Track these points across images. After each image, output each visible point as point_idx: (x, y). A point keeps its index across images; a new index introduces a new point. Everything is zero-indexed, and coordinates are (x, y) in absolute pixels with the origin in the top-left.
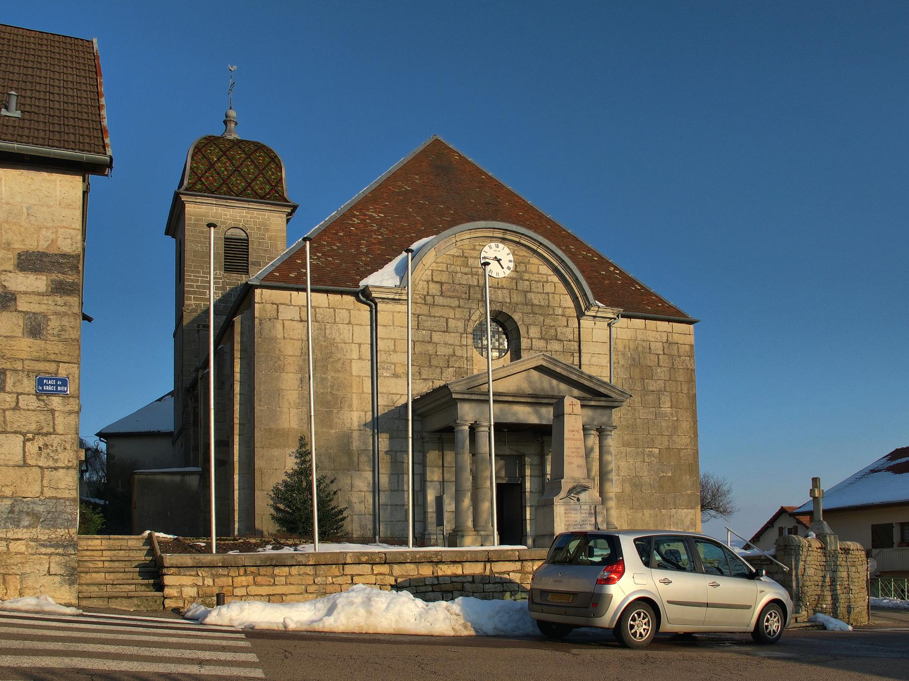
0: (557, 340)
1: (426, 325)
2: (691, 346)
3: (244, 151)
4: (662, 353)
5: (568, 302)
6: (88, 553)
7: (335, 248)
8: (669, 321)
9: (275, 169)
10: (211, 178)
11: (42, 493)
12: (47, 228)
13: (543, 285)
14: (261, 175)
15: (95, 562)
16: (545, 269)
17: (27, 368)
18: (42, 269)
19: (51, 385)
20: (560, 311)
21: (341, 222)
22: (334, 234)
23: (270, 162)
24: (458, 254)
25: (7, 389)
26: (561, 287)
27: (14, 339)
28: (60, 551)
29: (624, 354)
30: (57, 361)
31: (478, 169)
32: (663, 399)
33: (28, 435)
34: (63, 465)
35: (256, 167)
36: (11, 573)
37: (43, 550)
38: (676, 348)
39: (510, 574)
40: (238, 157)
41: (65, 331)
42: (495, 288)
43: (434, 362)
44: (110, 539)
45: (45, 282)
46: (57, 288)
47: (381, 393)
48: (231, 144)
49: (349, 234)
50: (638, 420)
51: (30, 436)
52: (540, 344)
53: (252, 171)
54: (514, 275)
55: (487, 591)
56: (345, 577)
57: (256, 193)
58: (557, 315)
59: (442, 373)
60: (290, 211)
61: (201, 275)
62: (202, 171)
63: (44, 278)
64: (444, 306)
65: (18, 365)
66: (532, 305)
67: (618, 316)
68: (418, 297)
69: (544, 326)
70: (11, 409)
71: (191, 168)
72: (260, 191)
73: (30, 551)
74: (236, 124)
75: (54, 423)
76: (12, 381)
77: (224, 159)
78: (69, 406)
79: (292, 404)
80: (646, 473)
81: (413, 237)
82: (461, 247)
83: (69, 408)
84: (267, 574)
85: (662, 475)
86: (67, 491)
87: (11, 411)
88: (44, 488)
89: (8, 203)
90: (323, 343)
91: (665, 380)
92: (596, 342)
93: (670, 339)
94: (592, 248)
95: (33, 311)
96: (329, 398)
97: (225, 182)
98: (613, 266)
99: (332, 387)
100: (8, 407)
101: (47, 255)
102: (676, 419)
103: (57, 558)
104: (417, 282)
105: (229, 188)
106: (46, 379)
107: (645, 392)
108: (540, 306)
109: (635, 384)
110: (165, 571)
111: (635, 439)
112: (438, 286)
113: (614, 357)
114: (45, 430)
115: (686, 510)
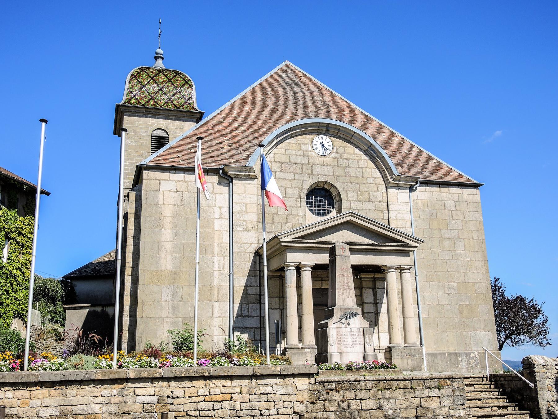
3: (166, 77)
26: (371, 164)
42: (321, 165)
43: (276, 220)
48: (157, 72)
53: (171, 90)
57: (174, 105)
58: (369, 183)
59: (282, 226)
66: (350, 176)
69: (360, 191)
72: (177, 104)
85: (461, 303)
115: (484, 332)
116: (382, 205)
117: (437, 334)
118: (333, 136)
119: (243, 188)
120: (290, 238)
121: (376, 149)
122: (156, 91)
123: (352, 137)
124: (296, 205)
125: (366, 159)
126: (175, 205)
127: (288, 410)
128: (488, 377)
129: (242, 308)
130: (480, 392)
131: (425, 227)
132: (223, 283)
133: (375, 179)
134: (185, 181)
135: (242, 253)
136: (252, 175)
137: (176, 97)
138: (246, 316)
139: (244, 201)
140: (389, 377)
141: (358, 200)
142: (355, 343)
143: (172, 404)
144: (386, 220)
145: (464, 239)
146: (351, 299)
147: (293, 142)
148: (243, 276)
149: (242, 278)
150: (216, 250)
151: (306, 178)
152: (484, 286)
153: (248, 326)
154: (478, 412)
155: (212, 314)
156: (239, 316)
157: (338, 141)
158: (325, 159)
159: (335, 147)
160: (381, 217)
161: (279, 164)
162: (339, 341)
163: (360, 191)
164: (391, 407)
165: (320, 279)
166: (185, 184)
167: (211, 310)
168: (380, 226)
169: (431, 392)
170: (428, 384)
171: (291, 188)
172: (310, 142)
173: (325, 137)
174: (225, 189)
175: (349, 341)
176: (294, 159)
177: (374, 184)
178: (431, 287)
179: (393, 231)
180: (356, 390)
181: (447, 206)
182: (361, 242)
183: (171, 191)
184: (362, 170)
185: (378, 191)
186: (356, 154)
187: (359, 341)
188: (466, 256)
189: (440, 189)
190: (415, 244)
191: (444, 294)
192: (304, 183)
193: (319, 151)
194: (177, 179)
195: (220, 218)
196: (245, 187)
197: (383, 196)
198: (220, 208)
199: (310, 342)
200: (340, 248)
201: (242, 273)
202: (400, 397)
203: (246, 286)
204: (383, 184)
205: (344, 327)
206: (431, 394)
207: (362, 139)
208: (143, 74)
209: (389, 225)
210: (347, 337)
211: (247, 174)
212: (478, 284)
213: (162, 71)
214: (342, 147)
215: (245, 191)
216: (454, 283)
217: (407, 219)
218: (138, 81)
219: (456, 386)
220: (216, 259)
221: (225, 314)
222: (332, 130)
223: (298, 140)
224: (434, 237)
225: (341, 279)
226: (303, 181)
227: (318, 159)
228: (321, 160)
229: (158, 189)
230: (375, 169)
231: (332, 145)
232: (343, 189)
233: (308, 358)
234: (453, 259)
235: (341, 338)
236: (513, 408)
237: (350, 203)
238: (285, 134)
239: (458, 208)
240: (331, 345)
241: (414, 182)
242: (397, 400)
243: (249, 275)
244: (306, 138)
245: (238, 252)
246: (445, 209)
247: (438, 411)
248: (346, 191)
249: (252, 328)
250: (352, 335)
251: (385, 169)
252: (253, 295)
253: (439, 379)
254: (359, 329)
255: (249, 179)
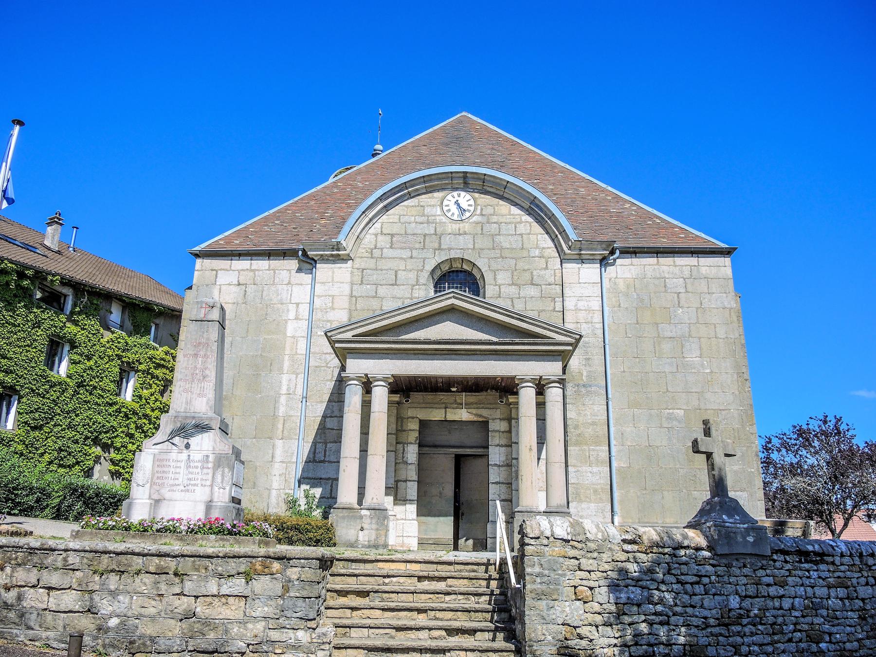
42: (455, 235)
66: (502, 249)
69: (516, 270)
116: (552, 289)
117: (644, 494)
118: (476, 191)
119: (330, 273)
120: (348, 335)
121: (542, 203)
123: (505, 189)
124: (411, 294)
125: (529, 221)
126: (234, 303)
128: (498, 563)
129: (315, 448)
130: (440, 593)
131: (629, 322)
132: (292, 413)
133: (542, 251)
134: (251, 270)
135: (322, 368)
136: (343, 255)
138: (320, 462)
139: (330, 293)
140: (121, 547)
141: (513, 284)
142: (192, 482)
144: (560, 312)
145: (700, 338)
146: (205, 400)
147: (413, 204)
148: (322, 402)
149: (319, 405)
150: (286, 364)
151: (430, 254)
152: (736, 415)
153: (323, 477)
154: (392, 637)
155: (273, 457)
156: (310, 462)
157: (483, 198)
158: (462, 225)
159: (479, 208)
160: (551, 308)
161: (388, 238)
162: (158, 478)
163: (516, 270)
164: (118, 611)
165: (444, 405)
166: (252, 274)
167: (271, 452)
168: (504, 312)
169: (225, 586)
170: (220, 569)
171: (404, 270)
172: (439, 203)
173: (463, 194)
174: (306, 278)
175: (182, 478)
176: (411, 228)
177: (540, 257)
178: (635, 417)
179: (527, 320)
180: (42, 567)
181: (670, 286)
183: (231, 285)
184: (522, 237)
185: (547, 268)
186: (513, 215)
187: (202, 480)
188: (702, 365)
189: (658, 260)
191: (659, 429)
192: (426, 262)
193: (453, 214)
194: (240, 268)
195: (297, 318)
196: (333, 272)
197: (555, 276)
198: (298, 304)
199: (373, 499)
200: (202, 307)
201: (319, 397)
202: (145, 591)
203: (324, 417)
204: (557, 257)
205: (176, 451)
206: (225, 590)
207: (520, 191)
210: (178, 470)
211: (335, 253)
212: (723, 413)
214: (490, 205)
215: (333, 278)
216: (678, 411)
217: (594, 308)
219: (294, 577)
220: (285, 378)
221: (291, 458)
222: (474, 182)
223: (421, 200)
224: (645, 337)
225: (190, 362)
226: (424, 259)
227: (450, 227)
228: (456, 226)
229: (214, 283)
230: (543, 234)
231: (473, 204)
232: (489, 267)
233: (364, 525)
234: (678, 371)
235: (164, 472)
236: (491, 634)
237: (500, 289)
238: (399, 192)
239: (690, 289)
240: (138, 485)
241: (606, 250)
242: (135, 598)
243: (329, 401)
244: (433, 197)
245: (316, 367)
246: (666, 291)
247: (235, 630)
248: (493, 270)
249: (329, 479)
250: (188, 467)
251: (557, 233)
252: (334, 429)
253: (249, 557)
254: (207, 456)
255: (340, 261)
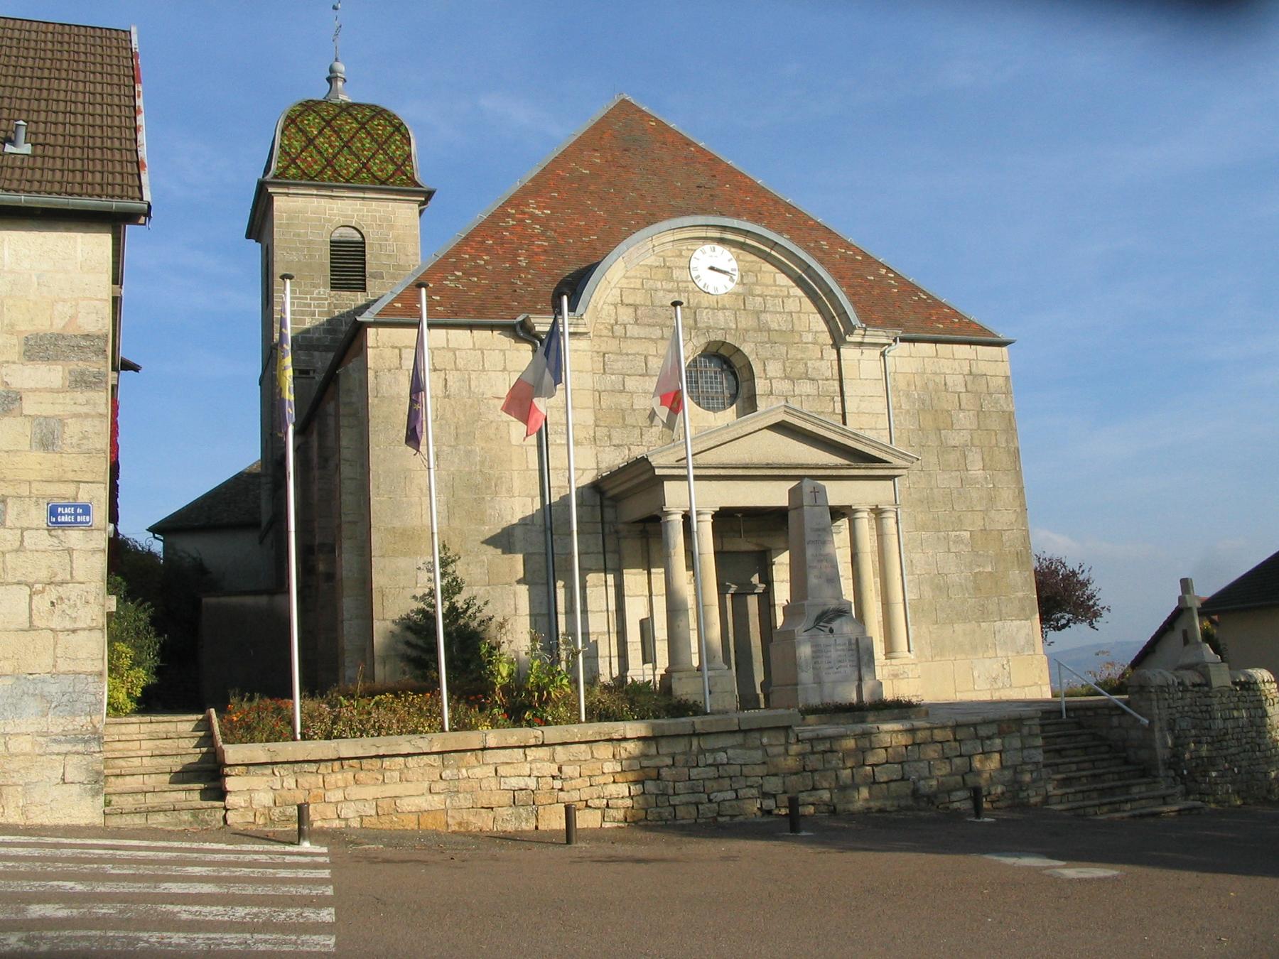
0: (809, 379)
1: (616, 367)
2: (1007, 378)
3: (356, 119)
4: (964, 390)
5: (819, 324)
6: (120, 745)
7: (482, 262)
8: (971, 343)
9: (401, 141)
10: (309, 159)
11: (54, 666)
12: (64, 301)
13: (783, 302)
14: (380, 151)
15: (129, 759)
16: (783, 279)
17: (36, 492)
18: (57, 356)
19: (68, 514)
20: (809, 337)
21: (491, 225)
22: (479, 242)
23: (394, 132)
24: (658, 264)
25: (8, 523)
26: (808, 305)
27: (18, 454)
28: (80, 748)
29: (908, 395)
30: (76, 481)
31: (683, 138)
32: (970, 458)
33: (36, 586)
34: (85, 626)
35: (373, 139)
36: (10, 783)
37: (56, 748)
38: (984, 381)
39: (729, 751)
40: (348, 127)
41: (88, 439)
42: (714, 309)
43: (630, 421)
44: (151, 722)
45: (61, 373)
46: (76, 381)
47: (554, 469)
48: (337, 110)
49: (502, 241)
50: (935, 491)
51: (39, 587)
52: (782, 386)
53: (368, 145)
54: (740, 289)
55: (694, 778)
56: (485, 768)
57: (375, 177)
58: (806, 343)
59: (642, 435)
60: (423, 199)
61: (298, 295)
62: (296, 148)
63: (60, 368)
64: (641, 338)
65: (24, 490)
66: (769, 330)
67: (895, 341)
68: (602, 327)
69: (788, 359)
70: (13, 551)
71: (281, 147)
72: (380, 173)
73: (37, 750)
74: (345, 81)
75: (72, 567)
76: (15, 513)
77: (327, 131)
78: (93, 542)
79: (424, 491)
80: (953, 569)
81: (593, 240)
82: (662, 254)
83: (93, 545)
84: (373, 768)
85: (977, 570)
86: (89, 662)
87: (14, 555)
88: (58, 660)
89: (12, 272)
90: (467, 400)
91: (971, 430)
92: (866, 379)
93: (974, 370)
94: (853, 243)
95: (44, 414)
96: (479, 479)
97: (329, 163)
98: (884, 266)
99: (482, 463)
100: (10, 548)
101: (63, 337)
102: (991, 486)
103: (77, 759)
104: (599, 306)
105: (335, 171)
106: (61, 506)
107: (944, 448)
108: (781, 331)
109: (927, 437)
110: (227, 770)
111: (934, 519)
112: (631, 310)
113: (894, 399)
114: (58, 579)
115: (1018, 622)
122: (336, 150)
127: (754, 792)
137: (377, 161)
143: (561, 790)
155: (516, 609)
160: (830, 410)
161: (631, 310)
167: (512, 602)
182: (803, 462)
186: (779, 286)
190: (904, 463)
197: (832, 369)
208: (309, 115)
209: (844, 423)
213: (348, 107)
217: (878, 412)
218: (301, 130)
245: (560, 487)
